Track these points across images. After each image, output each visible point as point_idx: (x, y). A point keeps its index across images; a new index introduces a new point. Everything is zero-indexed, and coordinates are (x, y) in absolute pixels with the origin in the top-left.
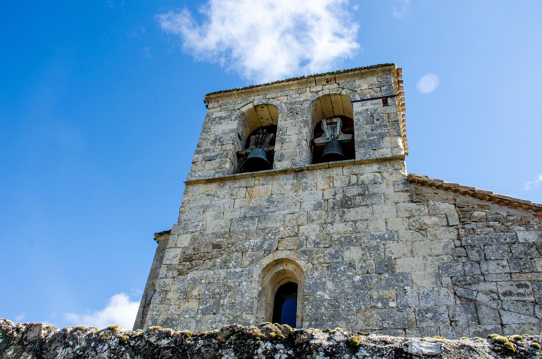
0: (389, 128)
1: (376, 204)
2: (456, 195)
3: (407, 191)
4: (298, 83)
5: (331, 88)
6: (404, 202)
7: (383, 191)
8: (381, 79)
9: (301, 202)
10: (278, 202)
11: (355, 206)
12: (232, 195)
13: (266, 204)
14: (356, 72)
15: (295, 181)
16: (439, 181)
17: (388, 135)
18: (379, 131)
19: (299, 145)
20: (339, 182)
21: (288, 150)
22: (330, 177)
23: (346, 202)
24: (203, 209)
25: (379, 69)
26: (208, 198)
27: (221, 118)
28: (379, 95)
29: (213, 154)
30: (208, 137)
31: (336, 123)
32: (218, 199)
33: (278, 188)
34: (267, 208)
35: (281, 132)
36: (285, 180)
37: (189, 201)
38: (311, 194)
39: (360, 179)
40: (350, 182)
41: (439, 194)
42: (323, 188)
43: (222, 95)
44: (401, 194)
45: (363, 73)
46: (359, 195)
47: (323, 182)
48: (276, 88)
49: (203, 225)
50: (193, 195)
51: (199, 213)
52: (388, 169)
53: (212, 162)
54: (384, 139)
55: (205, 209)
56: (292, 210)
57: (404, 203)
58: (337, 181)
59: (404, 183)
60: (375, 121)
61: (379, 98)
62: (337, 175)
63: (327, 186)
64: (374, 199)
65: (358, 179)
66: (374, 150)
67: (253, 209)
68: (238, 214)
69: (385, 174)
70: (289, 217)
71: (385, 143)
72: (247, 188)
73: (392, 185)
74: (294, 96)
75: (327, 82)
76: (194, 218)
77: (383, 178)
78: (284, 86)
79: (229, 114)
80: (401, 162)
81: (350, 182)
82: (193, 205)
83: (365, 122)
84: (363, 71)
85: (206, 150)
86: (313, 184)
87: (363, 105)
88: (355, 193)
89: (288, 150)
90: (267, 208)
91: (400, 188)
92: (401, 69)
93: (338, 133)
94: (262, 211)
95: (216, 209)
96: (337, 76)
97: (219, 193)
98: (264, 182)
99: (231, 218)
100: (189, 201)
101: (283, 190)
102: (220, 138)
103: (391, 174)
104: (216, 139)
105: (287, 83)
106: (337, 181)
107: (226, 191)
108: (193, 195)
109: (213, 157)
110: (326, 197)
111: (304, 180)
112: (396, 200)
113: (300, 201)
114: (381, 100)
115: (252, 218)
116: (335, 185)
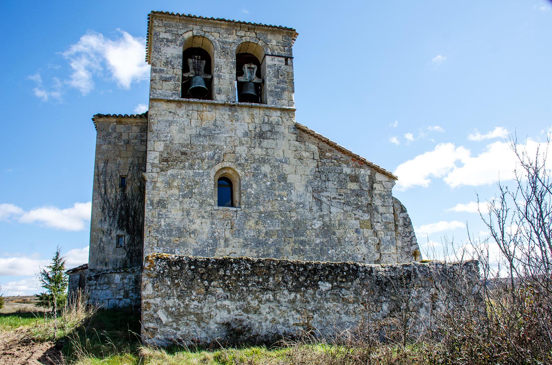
3: (295, 134)
5: (249, 37)
8: (285, 39)
12: (188, 115)
13: (213, 127)
15: (230, 113)
19: (231, 84)
20: (258, 119)
22: (252, 114)
25: (285, 31)
26: (170, 115)
28: (283, 53)
29: (168, 76)
30: (160, 58)
45: (275, 31)
46: (269, 131)
47: (248, 118)
48: (211, 23)
51: (166, 126)
53: (168, 83)
55: (170, 123)
59: (294, 128)
61: (283, 57)
62: (256, 114)
63: (250, 121)
65: (269, 119)
67: (205, 129)
68: (194, 132)
70: (228, 139)
74: (225, 36)
75: (249, 29)
77: (283, 122)
78: (217, 23)
82: (160, 118)
85: (161, 71)
87: (272, 60)
94: (211, 132)
95: (179, 125)
96: (256, 27)
102: (171, 61)
104: (167, 62)
107: (183, 111)
111: (236, 113)
112: (290, 138)
115: (205, 136)
116: (256, 121)
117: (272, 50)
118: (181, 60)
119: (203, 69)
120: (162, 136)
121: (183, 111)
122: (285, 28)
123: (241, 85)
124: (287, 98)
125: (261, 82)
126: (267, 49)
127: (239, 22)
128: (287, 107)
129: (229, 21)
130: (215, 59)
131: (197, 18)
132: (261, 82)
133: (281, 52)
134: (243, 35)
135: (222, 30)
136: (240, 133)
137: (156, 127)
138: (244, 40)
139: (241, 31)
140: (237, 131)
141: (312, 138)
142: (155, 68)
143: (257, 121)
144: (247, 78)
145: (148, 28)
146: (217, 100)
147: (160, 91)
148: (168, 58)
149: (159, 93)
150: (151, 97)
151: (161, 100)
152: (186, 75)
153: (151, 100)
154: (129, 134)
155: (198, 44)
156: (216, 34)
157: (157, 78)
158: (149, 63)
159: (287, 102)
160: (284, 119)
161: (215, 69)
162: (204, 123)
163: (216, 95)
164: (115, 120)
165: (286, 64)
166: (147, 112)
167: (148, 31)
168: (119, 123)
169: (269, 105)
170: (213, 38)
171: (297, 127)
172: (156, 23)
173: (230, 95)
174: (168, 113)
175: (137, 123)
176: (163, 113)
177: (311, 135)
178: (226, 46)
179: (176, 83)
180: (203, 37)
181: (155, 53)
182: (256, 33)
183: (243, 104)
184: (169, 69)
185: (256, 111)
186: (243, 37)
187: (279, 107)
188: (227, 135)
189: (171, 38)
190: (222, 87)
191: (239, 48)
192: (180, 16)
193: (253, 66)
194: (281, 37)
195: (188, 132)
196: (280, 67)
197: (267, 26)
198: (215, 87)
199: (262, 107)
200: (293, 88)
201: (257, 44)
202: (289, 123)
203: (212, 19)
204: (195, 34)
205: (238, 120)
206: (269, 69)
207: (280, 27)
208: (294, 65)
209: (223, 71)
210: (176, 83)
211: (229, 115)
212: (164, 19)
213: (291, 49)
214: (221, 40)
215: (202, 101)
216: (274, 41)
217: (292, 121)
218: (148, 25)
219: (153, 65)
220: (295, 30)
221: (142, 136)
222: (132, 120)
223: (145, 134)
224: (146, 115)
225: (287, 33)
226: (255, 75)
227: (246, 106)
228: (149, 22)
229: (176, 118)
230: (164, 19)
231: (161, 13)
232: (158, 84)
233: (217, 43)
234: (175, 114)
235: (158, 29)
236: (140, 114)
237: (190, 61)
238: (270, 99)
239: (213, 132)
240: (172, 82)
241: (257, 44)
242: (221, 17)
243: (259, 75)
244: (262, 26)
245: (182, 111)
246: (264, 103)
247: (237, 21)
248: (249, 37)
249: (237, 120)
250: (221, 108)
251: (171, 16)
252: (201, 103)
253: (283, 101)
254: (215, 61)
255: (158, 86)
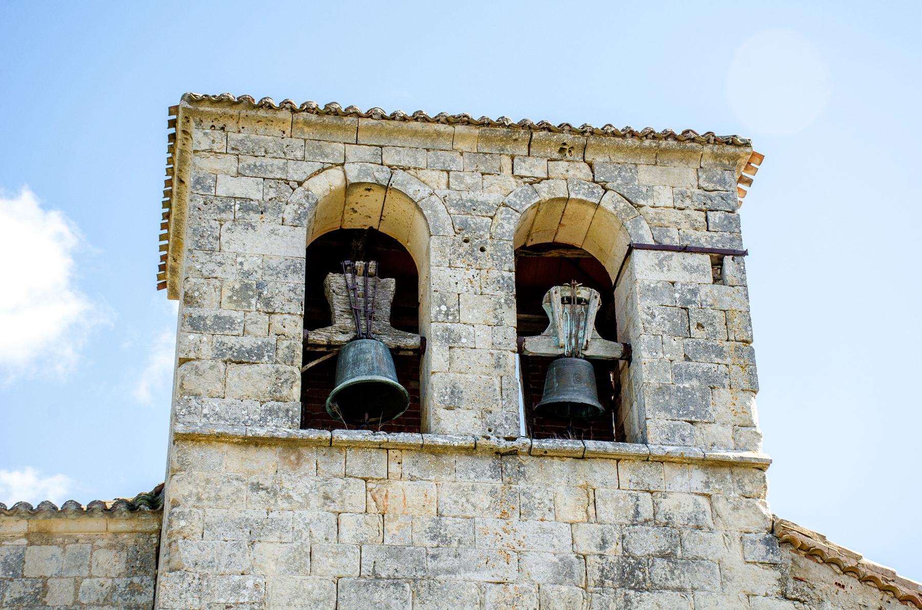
0: (728, 361)
1: (703, 589)
2: (886, 598)
3: (774, 565)
4: (481, 136)
5: (567, 178)
6: (767, 595)
7: (719, 555)
8: (709, 180)
9: (519, 553)
10: (460, 542)
11: (654, 588)
12: (326, 497)
13: (428, 543)
14: (647, 143)
15: (498, 484)
16: (850, 554)
17: (726, 382)
18: (706, 366)
19: (498, 366)
20: (610, 508)
21: (470, 377)
22: (586, 487)
23: (632, 573)
24: (247, 531)
25: (707, 149)
26: (255, 497)
27: (247, 205)
28: (703, 239)
29: (248, 342)
30: (219, 272)
31: (587, 302)
32: (286, 505)
33: (454, 497)
34: (434, 557)
35: (444, 308)
36: (472, 475)
37: (199, 499)
38: (544, 531)
39: (662, 507)
40: (637, 513)
41: (848, 589)
42: (571, 518)
43: (244, 113)
44: (758, 569)
45: (665, 151)
46: (663, 556)
47: (570, 501)
48: (415, 133)
49: (256, 586)
50: (208, 481)
51: (237, 545)
52: (727, 489)
53: (246, 368)
54: (715, 392)
55: (254, 533)
56: (499, 575)
57: (768, 599)
58: (605, 504)
59: (767, 542)
60: (693, 329)
61: (703, 251)
62: (604, 484)
63: (581, 516)
64: (698, 575)
65: (656, 505)
66: (692, 423)
67: (395, 553)
68: (350, 565)
69: (721, 505)
70: (493, 594)
71: (721, 409)
72: (366, 480)
73: (738, 540)
74: (468, 180)
75: (562, 150)
76: (224, 561)
77: (716, 515)
78: (439, 134)
79: (272, 194)
80: (759, 474)
81: (637, 513)
82: (214, 514)
83: (668, 325)
84: (663, 143)
85: (223, 323)
86: (547, 502)
87: (660, 264)
88: (652, 550)
89: (470, 377)
90: (434, 557)
91: (757, 553)
92: (762, 157)
93: (589, 336)
94: (419, 565)
95: (289, 537)
96: (592, 140)
97: (287, 485)
98: (416, 473)
99: (335, 572)
100: (199, 499)
101: (469, 506)
102: (260, 286)
103: (736, 509)
104: (246, 287)
105: (450, 129)
106: (605, 504)
107: (310, 481)
108: (208, 481)
109: (250, 352)
110: (583, 549)
111: (522, 485)
112: (750, 586)
113: (518, 548)
114: (706, 260)
115: (396, 582)
116: (602, 516)
117: (659, 226)
118: (299, 281)
119: (385, 310)
120: (218, 585)
121: (310, 481)
122: (710, 139)
123: (535, 372)
124: (730, 417)
125: (618, 354)
126: (636, 223)
127: (523, 125)
128: (732, 455)
129: (484, 123)
130: (434, 271)
131: (359, 116)
132: (618, 354)
133: (694, 235)
134: (540, 173)
135: (460, 159)
136: (539, 566)
137: (196, 551)
138: (545, 192)
139: (530, 160)
140: (529, 559)
141: (851, 582)
142: (195, 312)
143: (607, 512)
144: (563, 341)
145: (170, 161)
146: (443, 433)
147: (216, 404)
148: (248, 274)
149: (209, 415)
150: (180, 428)
151: (219, 438)
152: (320, 336)
153: (179, 439)
154: (77, 584)
155: (365, 213)
156: (435, 174)
157: (206, 351)
158: (174, 294)
159: (728, 432)
160: (721, 505)
161: (434, 310)
162: (391, 527)
163: (442, 412)
164: (21, 526)
165: (718, 279)
166: (159, 490)
167: (170, 172)
168: (43, 537)
169: (655, 447)
170: (424, 192)
171: (780, 536)
172: (200, 138)
173: (495, 409)
174: (246, 491)
175: (116, 534)
176: (227, 490)
177: (846, 571)
178: (474, 220)
179: (282, 367)
180: (386, 188)
181: (198, 253)
182: (591, 165)
183: (548, 444)
184: (253, 315)
185: (601, 474)
186: (539, 181)
187: (697, 452)
188: (485, 576)
189: (259, 196)
190: (462, 381)
191: (527, 228)
192: (293, 111)
193: (584, 293)
194: (692, 174)
195: (327, 565)
196: (694, 292)
197: (633, 134)
198: (434, 379)
199: (628, 458)
200: (752, 375)
201: (597, 206)
202: (742, 521)
203: (419, 117)
204: (352, 179)
205: (530, 513)
206: (648, 302)
207: (688, 137)
208: (749, 282)
209: (465, 316)
210: (282, 367)
211: (493, 493)
212: (231, 125)
213: (737, 221)
214: (455, 196)
215: (382, 437)
216: (665, 191)
217: (757, 511)
218: (171, 149)
219: (189, 300)
220: (747, 144)
221: (133, 590)
222: (96, 524)
223: (148, 579)
224: (154, 501)
225: (716, 156)
226: (591, 325)
227: (561, 455)
228: (173, 137)
229: (282, 511)
230: (231, 125)
231: (221, 101)
232: (210, 375)
233: (441, 207)
234: (272, 492)
235: (207, 164)
236: (130, 497)
237: (335, 281)
238: (655, 420)
239: (431, 564)
240: (265, 367)
241: (597, 206)
242: (452, 111)
243: (607, 325)
244: (615, 134)
245: (305, 479)
246: (634, 440)
247: (514, 120)
248: (567, 178)
249: (525, 513)
250: (463, 462)
251: (262, 113)
252: (380, 447)
253: (711, 428)
254: (434, 280)
255: (208, 383)
